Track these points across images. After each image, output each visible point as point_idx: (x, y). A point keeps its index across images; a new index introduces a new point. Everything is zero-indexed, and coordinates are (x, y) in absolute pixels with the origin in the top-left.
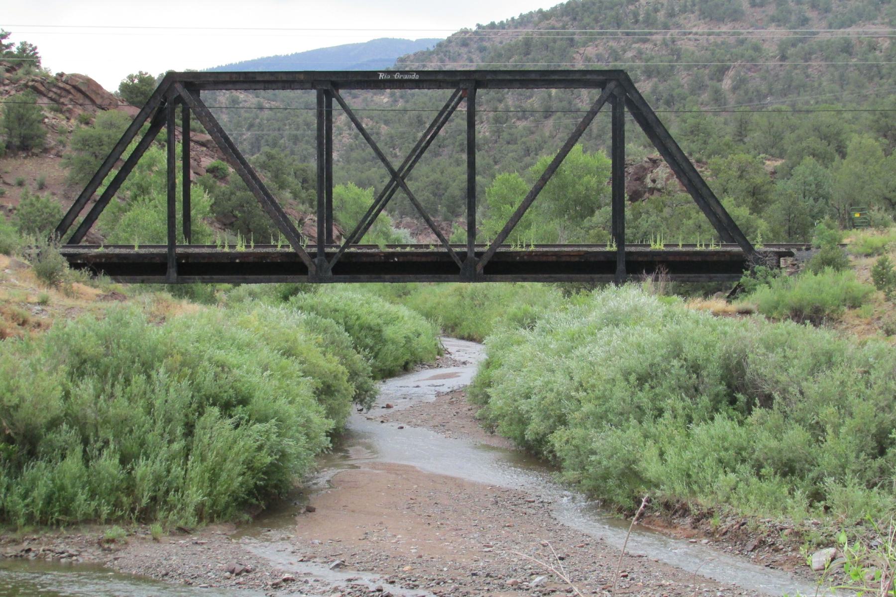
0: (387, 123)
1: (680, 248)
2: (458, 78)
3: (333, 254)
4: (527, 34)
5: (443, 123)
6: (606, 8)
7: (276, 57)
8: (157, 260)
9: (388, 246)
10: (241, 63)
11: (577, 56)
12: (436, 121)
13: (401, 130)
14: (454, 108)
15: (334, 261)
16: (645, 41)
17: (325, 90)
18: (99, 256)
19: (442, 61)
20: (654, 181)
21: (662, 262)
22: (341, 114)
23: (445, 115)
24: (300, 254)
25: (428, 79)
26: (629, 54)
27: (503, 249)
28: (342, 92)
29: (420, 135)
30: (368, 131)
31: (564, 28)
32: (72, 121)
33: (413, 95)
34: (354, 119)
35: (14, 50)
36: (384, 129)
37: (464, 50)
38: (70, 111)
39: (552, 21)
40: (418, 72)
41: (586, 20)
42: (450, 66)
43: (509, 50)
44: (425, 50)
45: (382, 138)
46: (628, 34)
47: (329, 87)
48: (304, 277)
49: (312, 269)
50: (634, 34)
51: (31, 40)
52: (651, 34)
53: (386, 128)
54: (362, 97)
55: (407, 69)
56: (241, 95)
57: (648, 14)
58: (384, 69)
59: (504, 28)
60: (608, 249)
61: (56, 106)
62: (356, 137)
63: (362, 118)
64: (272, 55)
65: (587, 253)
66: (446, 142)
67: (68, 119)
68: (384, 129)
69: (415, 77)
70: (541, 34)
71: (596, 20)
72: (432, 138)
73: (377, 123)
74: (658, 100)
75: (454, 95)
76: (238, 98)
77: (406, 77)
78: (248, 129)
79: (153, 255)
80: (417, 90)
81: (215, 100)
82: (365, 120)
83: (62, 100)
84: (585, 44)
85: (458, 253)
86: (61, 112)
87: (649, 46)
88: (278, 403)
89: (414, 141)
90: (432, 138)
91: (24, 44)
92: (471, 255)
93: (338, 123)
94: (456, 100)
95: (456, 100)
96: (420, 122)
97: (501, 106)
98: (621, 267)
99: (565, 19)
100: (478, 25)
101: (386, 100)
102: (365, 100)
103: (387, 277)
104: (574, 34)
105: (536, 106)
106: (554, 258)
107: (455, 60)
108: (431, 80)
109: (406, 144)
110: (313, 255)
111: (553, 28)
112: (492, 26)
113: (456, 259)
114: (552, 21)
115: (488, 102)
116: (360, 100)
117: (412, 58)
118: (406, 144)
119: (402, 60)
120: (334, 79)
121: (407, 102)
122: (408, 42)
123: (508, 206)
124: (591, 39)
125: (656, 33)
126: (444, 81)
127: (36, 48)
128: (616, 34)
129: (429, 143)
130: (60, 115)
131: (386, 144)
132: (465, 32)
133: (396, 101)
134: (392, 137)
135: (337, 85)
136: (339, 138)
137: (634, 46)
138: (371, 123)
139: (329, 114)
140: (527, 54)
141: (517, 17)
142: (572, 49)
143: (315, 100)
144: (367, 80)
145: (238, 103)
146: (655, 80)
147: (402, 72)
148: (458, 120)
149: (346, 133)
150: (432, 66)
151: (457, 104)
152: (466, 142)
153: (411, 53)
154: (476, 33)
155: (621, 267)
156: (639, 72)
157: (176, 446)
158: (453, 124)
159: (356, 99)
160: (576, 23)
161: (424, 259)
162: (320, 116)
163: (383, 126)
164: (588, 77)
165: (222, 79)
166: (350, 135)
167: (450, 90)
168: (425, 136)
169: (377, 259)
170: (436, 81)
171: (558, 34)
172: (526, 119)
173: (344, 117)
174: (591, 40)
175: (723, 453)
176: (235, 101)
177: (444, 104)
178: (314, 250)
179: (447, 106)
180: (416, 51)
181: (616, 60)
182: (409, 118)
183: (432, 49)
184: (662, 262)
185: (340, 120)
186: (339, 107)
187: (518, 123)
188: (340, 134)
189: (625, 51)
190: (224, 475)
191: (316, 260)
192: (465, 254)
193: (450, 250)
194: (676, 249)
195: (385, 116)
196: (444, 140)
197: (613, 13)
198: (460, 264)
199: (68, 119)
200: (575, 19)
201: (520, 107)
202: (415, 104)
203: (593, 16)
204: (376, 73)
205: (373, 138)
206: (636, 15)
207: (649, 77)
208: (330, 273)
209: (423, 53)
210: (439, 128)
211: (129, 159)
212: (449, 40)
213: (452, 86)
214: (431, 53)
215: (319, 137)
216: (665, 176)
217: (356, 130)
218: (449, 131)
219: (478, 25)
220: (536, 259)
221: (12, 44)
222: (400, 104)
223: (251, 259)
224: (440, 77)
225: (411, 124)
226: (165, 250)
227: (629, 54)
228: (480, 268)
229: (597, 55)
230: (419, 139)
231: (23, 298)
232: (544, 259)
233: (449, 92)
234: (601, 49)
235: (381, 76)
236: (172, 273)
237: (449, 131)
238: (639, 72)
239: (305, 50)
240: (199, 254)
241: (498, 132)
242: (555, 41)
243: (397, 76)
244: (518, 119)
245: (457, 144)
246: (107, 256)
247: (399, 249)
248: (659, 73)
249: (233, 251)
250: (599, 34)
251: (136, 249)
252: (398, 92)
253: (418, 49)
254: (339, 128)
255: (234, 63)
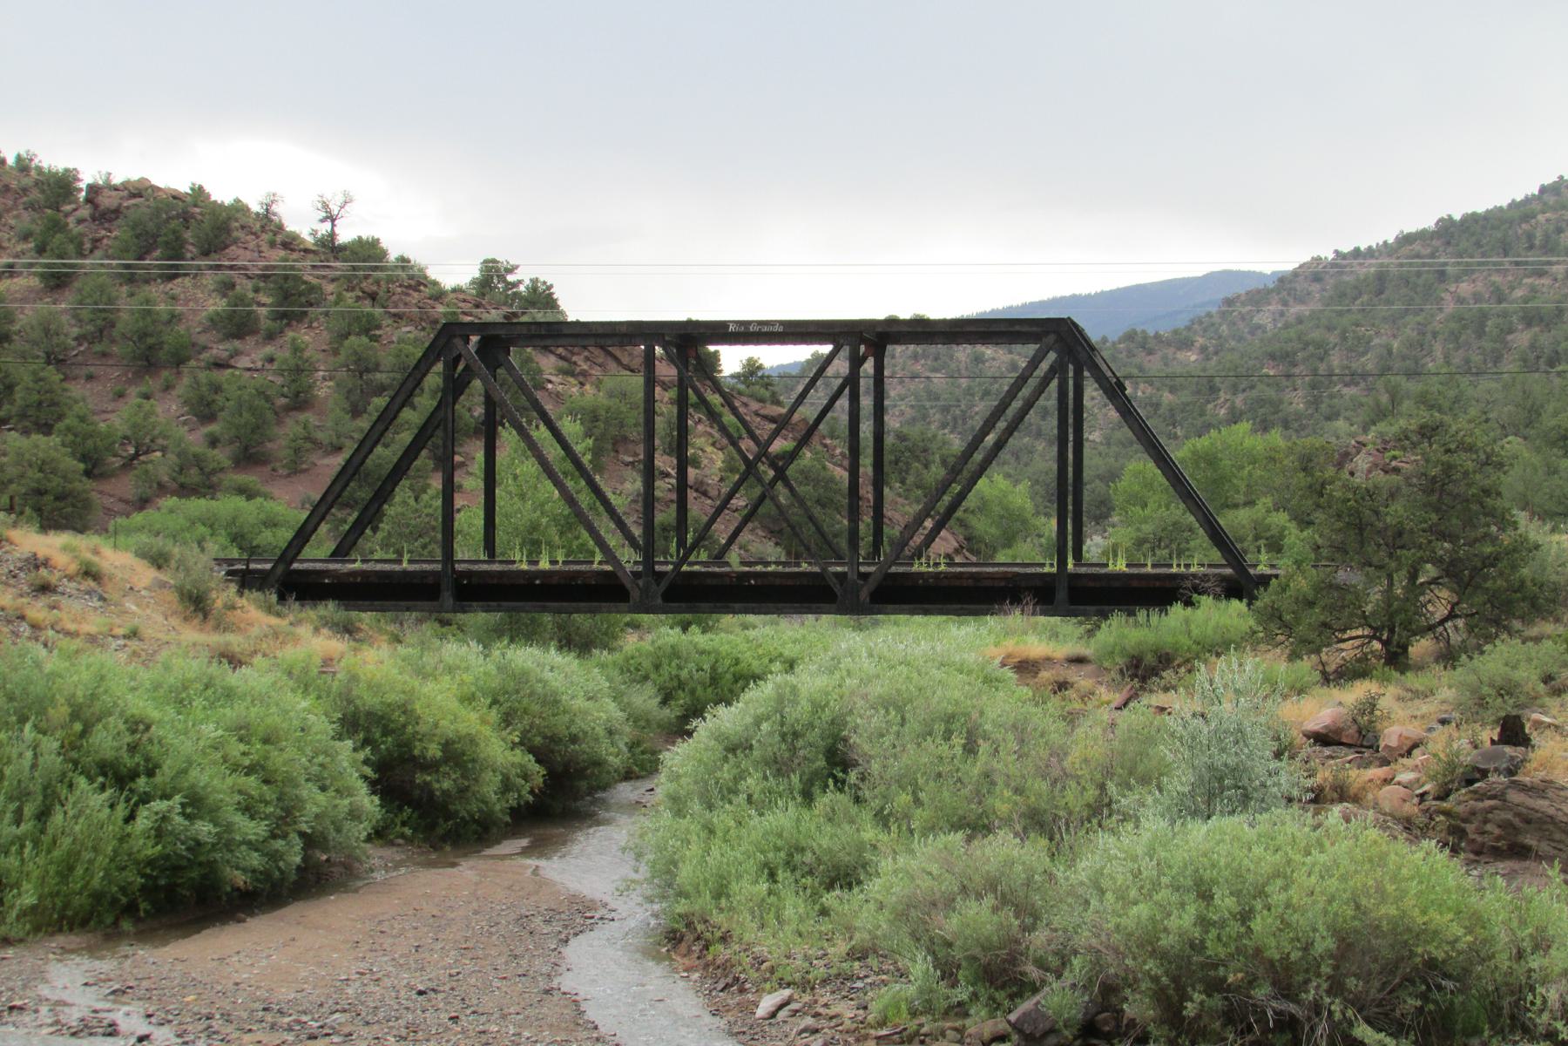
0: (1173, 390)
1: (1149, 569)
3: (666, 573)
4: (1382, 265)
6: (1493, 228)
7: (1074, 297)
8: (430, 580)
9: (743, 563)
10: (1024, 306)
11: (1447, 296)
15: (664, 584)
16: (1541, 274)
18: (354, 573)
20: (1352, 474)
21: (1029, 589)
24: (620, 574)
26: (1519, 293)
27: (901, 569)
31: (1432, 256)
32: (588, 387)
35: (522, 288)
37: (1315, 287)
38: (584, 374)
39: (1417, 247)
41: (1464, 244)
43: (1356, 287)
44: (1261, 287)
46: (1517, 263)
48: (623, 606)
49: (635, 594)
50: (1526, 263)
51: (545, 276)
52: (1549, 263)
56: (988, 351)
57: (1547, 237)
59: (1372, 256)
60: (1047, 569)
61: (564, 365)
64: (1067, 293)
65: (1018, 574)
67: (582, 384)
70: (1401, 265)
71: (1478, 244)
74: (1538, 358)
76: (983, 354)
78: (982, 399)
79: (424, 573)
81: (951, 357)
83: (574, 358)
84: (1458, 279)
85: (836, 574)
86: (573, 374)
87: (1546, 281)
91: (535, 281)
92: (853, 576)
97: (1322, 368)
98: (1061, 594)
99: (1435, 243)
100: (1336, 252)
101: (1193, 358)
103: (737, 606)
104: (1446, 264)
105: (1370, 367)
106: (971, 582)
107: (1302, 302)
110: (636, 575)
111: (1418, 256)
112: (1356, 253)
113: (833, 582)
114: (1417, 247)
115: (1305, 360)
122: (1261, 275)
123: (1138, 508)
124: (1467, 272)
125: (1558, 263)
127: (551, 287)
128: (1501, 264)
130: (571, 380)
132: (1317, 260)
137: (1526, 281)
138: (1149, 390)
140: (1381, 292)
141: (1391, 240)
142: (1443, 286)
145: (983, 362)
146: (1537, 329)
154: (1333, 265)
155: (1061, 594)
156: (1515, 319)
157: (25, 827)
160: (1450, 249)
161: (790, 582)
164: (1017, 328)
165: (994, 328)
169: (727, 581)
171: (1424, 265)
172: (1357, 384)
174: (1465, 273)
175: (771, 855)
176: (978, 359)
178: (640, 568)
181: (1500, 302)
183: (1271, 286)
184: (1029, 589)
187: (1346, 391)
189: (1513, 288)
190: (79, 871)
191: (641, 583)
192: (844, 574)
193: (824, 569)
194: (1142, 571)
197: (1499, 235)
198: (837, 589)
199: (582, 384)
200: (1448, 243)
201: (1348, 368)
203: (1474, 239)
206: (1530, 237)
207: (1529, 325)
208: (659, 601)
209: (1259, 291)
212: (1295, 274)
214: (1269, 292)
216: (1366, 466)
219: (1336, 252)
220: (946, 583)
221: (520, 282)
223: (555, 581)
225: (1198, 392)
226: (438, 567)
227: (1519, 293)
228: (864, 594)
229: (1475, 294)
231: (105, 629)
232: (958, 583)
234: (1480, 287)
236: (447, 598)
238: (1515, 319)
239: (1114, 287)
240: (486, 572)
241: (1315, 402)
242: (1419, 274)
244: (1346, 385)
246: (363, 573)
247: (759, 568)
248: (1541, 320)
249: (533, 568)
250: (1479, 264)
251: (405, 565)
253: (1254, 285)
255: (1015, 304)
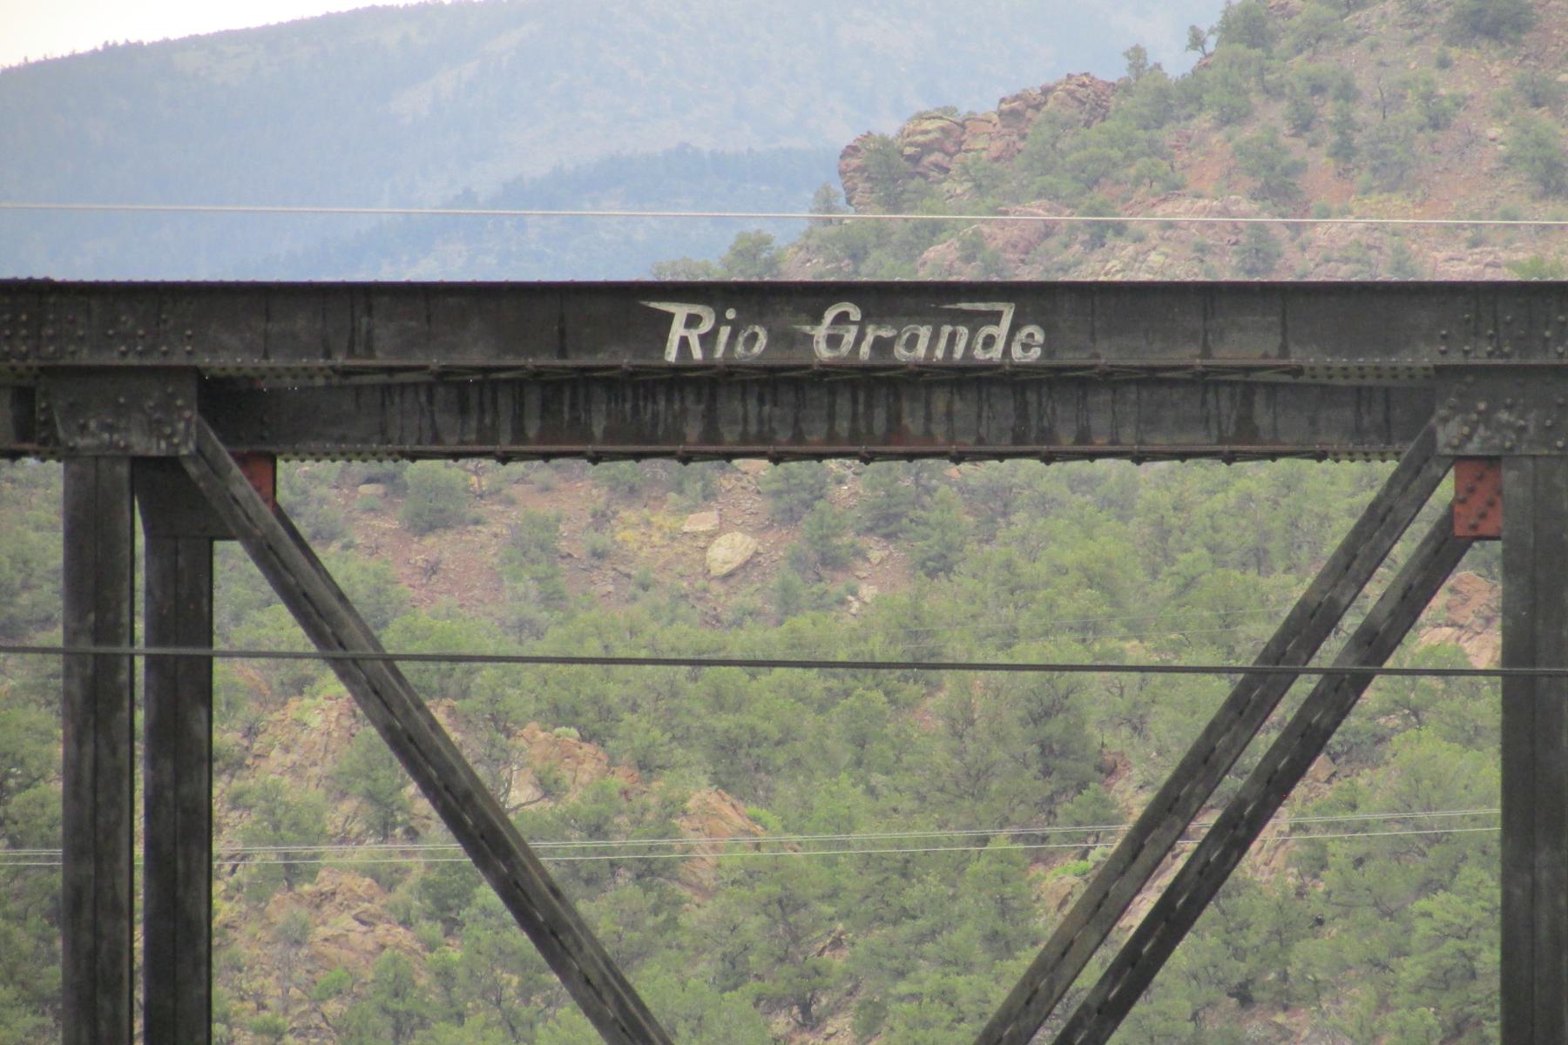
0: (739, 764)
2: (1425, 356)
5: (1277, 784)
12: (1202, 765)
13: (869, 833)
14: (1376, 644)
17: (140, 463)
19: (1280, 186)
22: (300, 686)
23: (1291, 705)
25: (1127, 368)
28: (310, 485)
29: (1063, 880)
30: (553, 855)
33: (1000, 503)
34: (415, 746)
36: (718, 831)
40: (1035, 299)
42: (1344, 237)
44: (1114, 70)
45: (697, 915)
47: (185, 435)
53: (732, 814)
54: (499, 523)
55: (937, 263)
58: (717, 271)
62: (445, 908)
63: (501, 722)
66: (1310, 953)
68: (718, 831)
69: (1010, 342)
72: (1172, 921)
73: (646, 766)
75: (1379, 523)
77: (921, 345)
80: (1030, 466)
82: (534, 741)
88: (885, 553)
89: (999, 944)
90: (1172, 921)
93: (272, 771)
94: (1404, 550)
95: (1404, 550)
96: (1065, 764)
101: (729, 550)
102: (534, 546)
107: (1393, 174)
108: (1150, 378)
109: (929, 977)
116: (480, 545)
117: (983, 147)
118: (929, 977)
119: (887, 169)
120: (229, 356)
121: (938, 566)
126: (1289, 387)
129: (1137, 970)
131: (733, 973)
133: (830, 561)
134: (786, 904)
135: (256, 420)
136: (283, 908)
138: (586, 775)
139: (186, 689)
143: (51, 549)
144: (553, 370)
147: (885, 299)
148: (1423, 747)
149: (345, 865)
150: (1170, 237)
151: (1409, 604)
152: (1490, 958)
153: (982, 101)
158: (1376, 786)
159: (434, 545)
162: (93, 702)
163: (701, 794)
166: (386, 879)
167: (1346, 471)
168: (1101, 906)
170: (1205, 381)
173: (326, 707)
177: (1289, 589)
179: (1312, 621)
180: (1032, 79)
182: (960, 724)
183: (1176, 62)
185: (285, 739)
186: (280, 626)
188: (292, 873)
195: (718, 702)
196: (1283, 935)
202: (1014, 586)
204: (629, 304)
205: (600, 914)
209: (1091, 100)
210: (1238, 831)
211: (1310, 760)
213: (1360, 444)
214: (1168, 103)
215: (87, 907)
217: (441, 841)
218: (1340, 849)
222: (873, 597)
224: (1246, 345)
225: (976, 779)
230: (1046, 923)
233: (1341, 488)
235: (686, 335)
237: (1340, 849)
243: (833, 339)
245: (1412, 970)
252: (848, 483)
254: (282, 822)
